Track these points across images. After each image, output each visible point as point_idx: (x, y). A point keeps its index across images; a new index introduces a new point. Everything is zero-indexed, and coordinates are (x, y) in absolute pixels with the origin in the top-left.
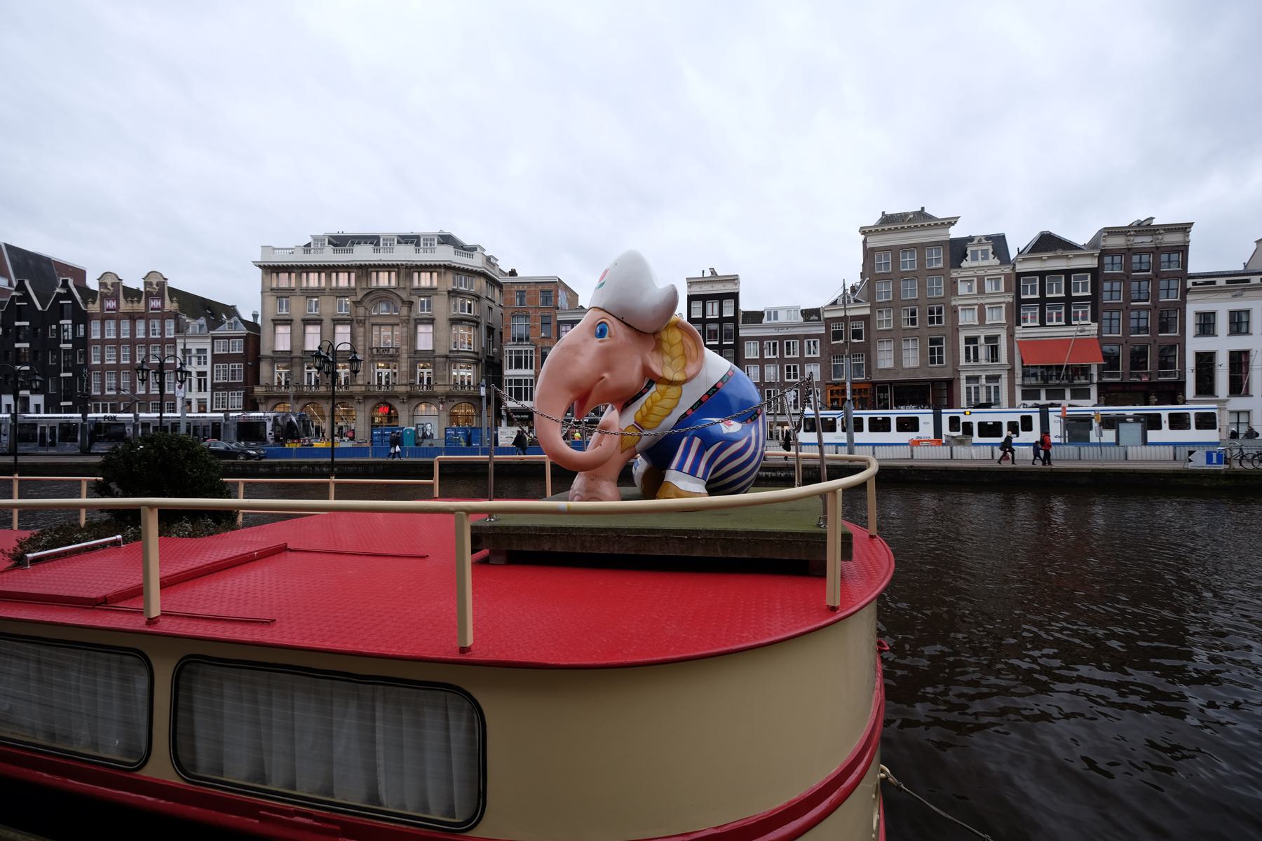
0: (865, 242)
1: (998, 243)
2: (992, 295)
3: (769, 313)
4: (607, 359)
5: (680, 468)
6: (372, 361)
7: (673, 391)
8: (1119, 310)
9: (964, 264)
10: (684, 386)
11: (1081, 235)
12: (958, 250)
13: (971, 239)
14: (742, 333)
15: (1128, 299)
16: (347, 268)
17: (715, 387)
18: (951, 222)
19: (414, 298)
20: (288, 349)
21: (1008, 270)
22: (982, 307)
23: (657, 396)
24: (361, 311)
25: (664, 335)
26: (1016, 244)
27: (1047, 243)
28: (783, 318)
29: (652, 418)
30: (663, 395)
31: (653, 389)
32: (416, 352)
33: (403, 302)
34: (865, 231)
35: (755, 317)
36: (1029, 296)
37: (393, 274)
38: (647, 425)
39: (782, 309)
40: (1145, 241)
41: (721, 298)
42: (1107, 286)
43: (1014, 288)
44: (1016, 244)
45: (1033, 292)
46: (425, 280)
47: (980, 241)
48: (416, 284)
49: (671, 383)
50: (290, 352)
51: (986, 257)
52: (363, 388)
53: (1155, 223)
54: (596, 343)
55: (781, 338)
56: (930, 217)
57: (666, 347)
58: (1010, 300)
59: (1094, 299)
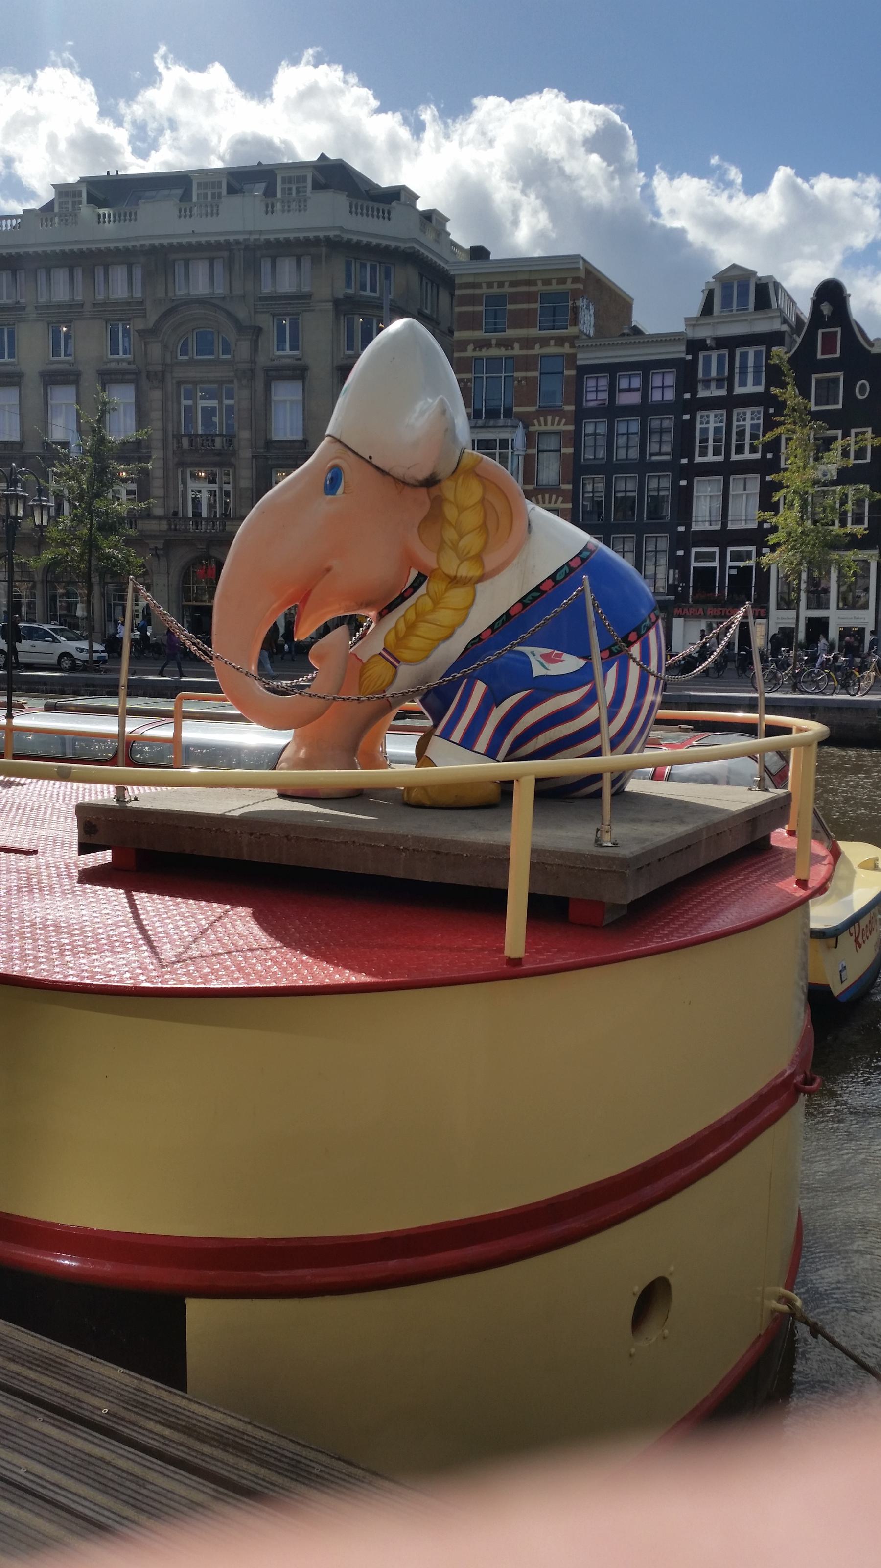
6: (182, 464)
7: (457, 596)
10: (479, 586)
16: (124, 256)
19: (265, 321)
20: (16, 437)
23: (428, 603)
24: (156, 351)
25: (448, 489)
32: (269, 444)
33: (240, 328)
37: (219, 267)
38: (405, 654)
46: (286, 278)
48: (267, 289)
49: (454, 581)
50: (21, 444)
52: (164, 526)
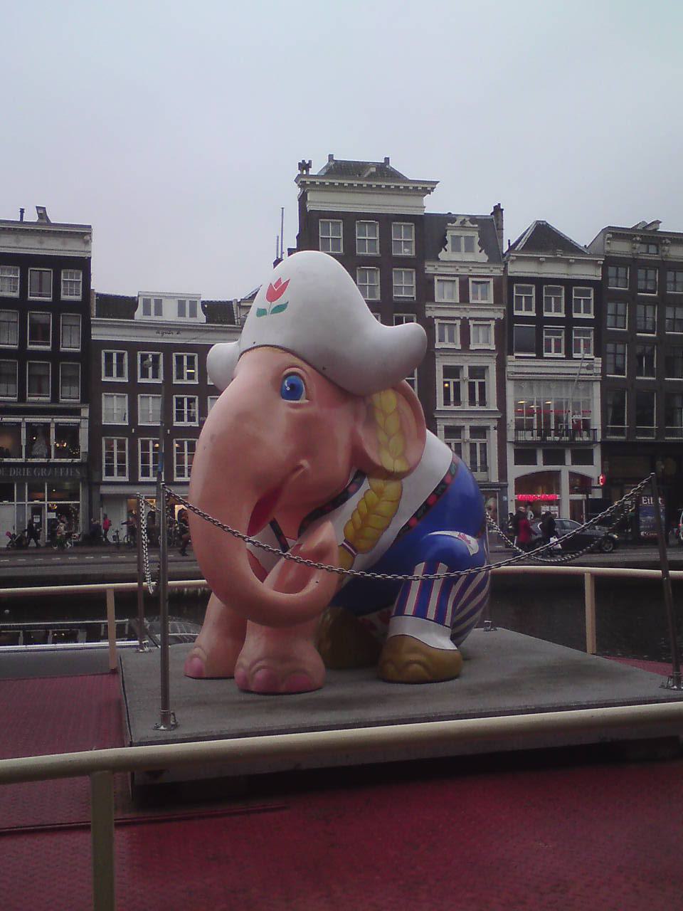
0: (303, 200)
1: (490, 226)
2: (480, 307)
3: (147, 303)
4: (307, 435)
5: (421, 612)
7: (391, 488)
8: (623, 342)
9: (443, 255)
11: (582, 233)
12: (432, 231)
13: (450, 218)
14: (98, 334)
15: (634, 328)
17: (443, 482)
18: (426, 188)
21: (498, 272)
22: (465, 323)
23: (372, 495)
26: (514, 230)
27: (544, 238)
28: (170, 314)
29: (369, 532)
30: (380, 493)
31: (366, 485)
34: (306, 183)
35: (121, 307)
36: (523, 313)
39: (170, 297)
40: (651, 254)
41: (58, 264)
42: (611, 308)
43: (505, 299)
44: (514, 230)
45: (528, 308)
47: (463, 222)
51: (469, 249)
53: (662, 228)
54: (284, 408)
55: (168, 349)
56: (395, 176)
57: (379, 418)
58: (501, 315)
59: (598, 323)
